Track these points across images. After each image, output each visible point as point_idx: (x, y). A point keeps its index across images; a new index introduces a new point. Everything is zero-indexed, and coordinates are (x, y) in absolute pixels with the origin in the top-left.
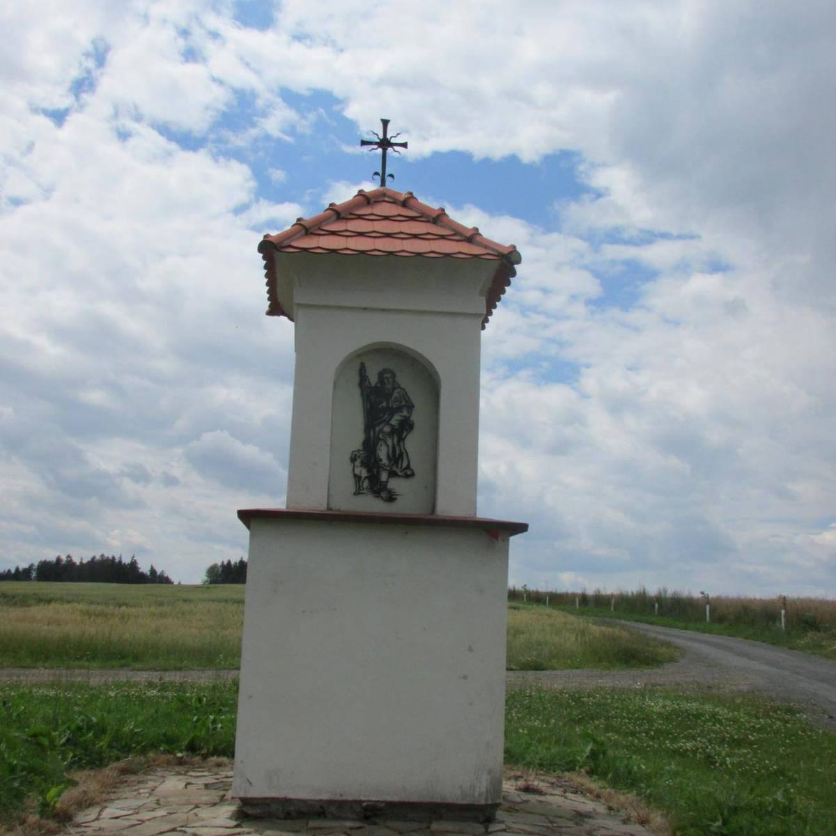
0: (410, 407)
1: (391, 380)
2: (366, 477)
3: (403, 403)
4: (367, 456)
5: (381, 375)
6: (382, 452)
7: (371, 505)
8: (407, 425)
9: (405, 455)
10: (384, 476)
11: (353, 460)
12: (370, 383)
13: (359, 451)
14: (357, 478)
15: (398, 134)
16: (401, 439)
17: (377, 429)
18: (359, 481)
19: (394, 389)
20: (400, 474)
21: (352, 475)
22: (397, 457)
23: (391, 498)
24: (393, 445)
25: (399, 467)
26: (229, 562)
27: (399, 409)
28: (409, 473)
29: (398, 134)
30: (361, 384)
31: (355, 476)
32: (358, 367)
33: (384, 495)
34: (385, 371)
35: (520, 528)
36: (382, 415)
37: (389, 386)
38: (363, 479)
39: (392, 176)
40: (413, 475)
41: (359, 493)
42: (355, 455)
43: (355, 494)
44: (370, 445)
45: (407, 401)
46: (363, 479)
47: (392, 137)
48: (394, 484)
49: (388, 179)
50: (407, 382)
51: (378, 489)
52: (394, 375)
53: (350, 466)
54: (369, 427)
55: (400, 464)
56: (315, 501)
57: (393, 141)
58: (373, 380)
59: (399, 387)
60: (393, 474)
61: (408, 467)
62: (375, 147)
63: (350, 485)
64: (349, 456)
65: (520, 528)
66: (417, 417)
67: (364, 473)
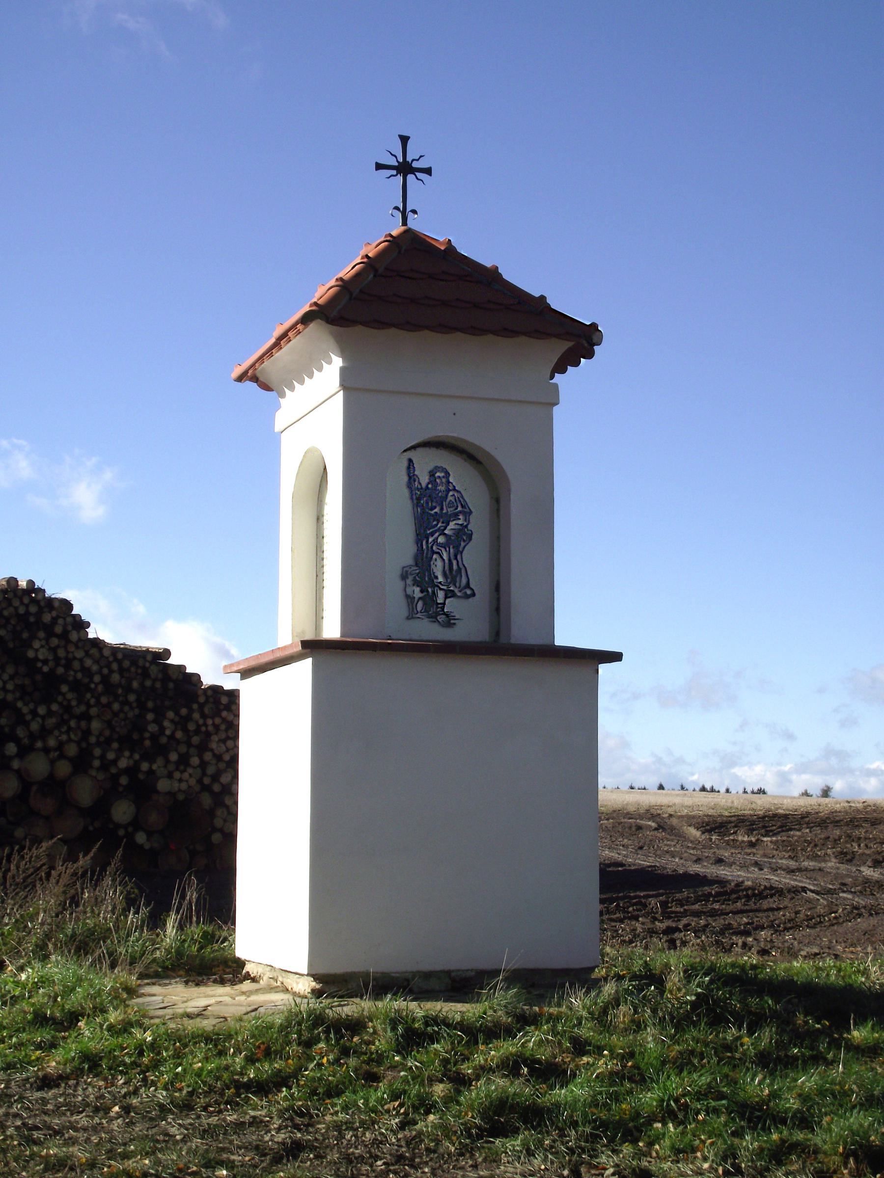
0: (468, 513)
1: (444, 480)
2: (420, 598)
3: (459, 509)
4: (419, 571)
5: (432, 474)
6: (438, 568)
7: (426, 630)
8: (463, 535)
9: (463, 571)
10: (441, 595)
11: (404, 577)
12: (420, 484)
13: (410, 566)
14: (409, 598)
15: (421, 156)
16: (458, 552)
17: (431, 540)
18: (412, 604)
19: (448, 490)
20: (459, 594)
21: (401, 595)
22: (453, 574)
23: (449, 621)
24: (450, 560)
25: (458, 585)
26: (167, 653)
27: (456, 516)
28: (469, 592)
29: (421, 156)
30: (410, 485)
31: (407, 596)
32: (405, 464)
33: (441, 618)
34: (437, 469)
35: (616, 657)
36: (435, 523)
37: (441, 488)
38: (416, 600)
39: (414, 212)
40: (473, 595)
41: (413, 618)
42: (407, 571)
43: (408, 618)
44: (422, 559)
45: (462, 506)
46: (416, 600)
47: (413, 160)
48: (451, 605)
49: (410, 216)
50: (463, 480)
51: (434, 611)
52: (447, 474)
53: (401, 584)
54: (421, 536)
55: (458, 579)
56: (365, 634)
57: (415, 165)
58: (424, 480)
59: (454, 489)
60: (449, 594)
61: (468, 586)
62: (394, 172)
63: (403, 609)
64: (399, 572)
65: (616, 657)
66: (479, 524)
67: (417, 592)
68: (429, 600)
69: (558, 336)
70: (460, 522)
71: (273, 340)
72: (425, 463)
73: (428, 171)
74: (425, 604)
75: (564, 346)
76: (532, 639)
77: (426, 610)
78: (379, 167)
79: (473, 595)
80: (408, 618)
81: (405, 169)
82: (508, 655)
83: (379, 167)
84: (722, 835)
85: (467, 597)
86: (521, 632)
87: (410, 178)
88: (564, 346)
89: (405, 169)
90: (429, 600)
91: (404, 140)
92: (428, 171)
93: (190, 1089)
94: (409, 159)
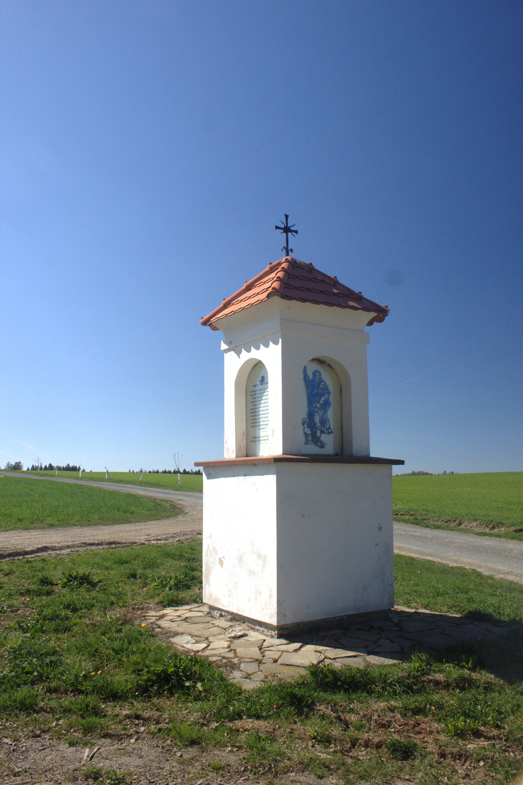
0: (329, 393)
4: (309, 422)
6: (317, 419)
8: (327, 404)
11: (303, 424)
16: (325, 412)
20: (326, 432)
22: (324, 422)
28: (330, 431)
31: (305, 433)
33: (319, 444)
43: (305, 444)
44: (311, 415)
50: (326, 377)
51: (316, 440)
52: (320, 374)
53: (301, 427)
57: (292, 228)
58: (311, 376)
60: (322, 432)
61: (329, 428)
68: (314, 435)
69: (374, 311)
70: (326, 397)
71: (222, 305)
72: (315, 367)
73: (296, 232)
74: (312, 437)
75: (373, 314)
76: (362, 454)
77: (312, 440)
78: (277, 228)
79: (332, 432)
80: (305, 444)
81: (287, 230)
82: (339, 463)
83: (277, 228)
84: (28, 560)
85: (329, 433)
86: (356, 449)
87: (290, 234)
88: (373, 314)
89: (287, 230)
90: (314, 435)
91: (287, 217)
92: (296, 232)
93: (506, 738)
94: (289, 225)
